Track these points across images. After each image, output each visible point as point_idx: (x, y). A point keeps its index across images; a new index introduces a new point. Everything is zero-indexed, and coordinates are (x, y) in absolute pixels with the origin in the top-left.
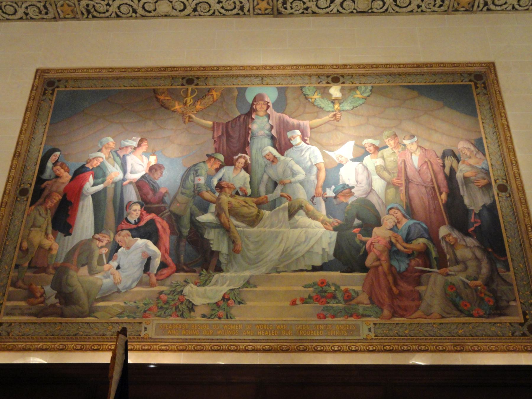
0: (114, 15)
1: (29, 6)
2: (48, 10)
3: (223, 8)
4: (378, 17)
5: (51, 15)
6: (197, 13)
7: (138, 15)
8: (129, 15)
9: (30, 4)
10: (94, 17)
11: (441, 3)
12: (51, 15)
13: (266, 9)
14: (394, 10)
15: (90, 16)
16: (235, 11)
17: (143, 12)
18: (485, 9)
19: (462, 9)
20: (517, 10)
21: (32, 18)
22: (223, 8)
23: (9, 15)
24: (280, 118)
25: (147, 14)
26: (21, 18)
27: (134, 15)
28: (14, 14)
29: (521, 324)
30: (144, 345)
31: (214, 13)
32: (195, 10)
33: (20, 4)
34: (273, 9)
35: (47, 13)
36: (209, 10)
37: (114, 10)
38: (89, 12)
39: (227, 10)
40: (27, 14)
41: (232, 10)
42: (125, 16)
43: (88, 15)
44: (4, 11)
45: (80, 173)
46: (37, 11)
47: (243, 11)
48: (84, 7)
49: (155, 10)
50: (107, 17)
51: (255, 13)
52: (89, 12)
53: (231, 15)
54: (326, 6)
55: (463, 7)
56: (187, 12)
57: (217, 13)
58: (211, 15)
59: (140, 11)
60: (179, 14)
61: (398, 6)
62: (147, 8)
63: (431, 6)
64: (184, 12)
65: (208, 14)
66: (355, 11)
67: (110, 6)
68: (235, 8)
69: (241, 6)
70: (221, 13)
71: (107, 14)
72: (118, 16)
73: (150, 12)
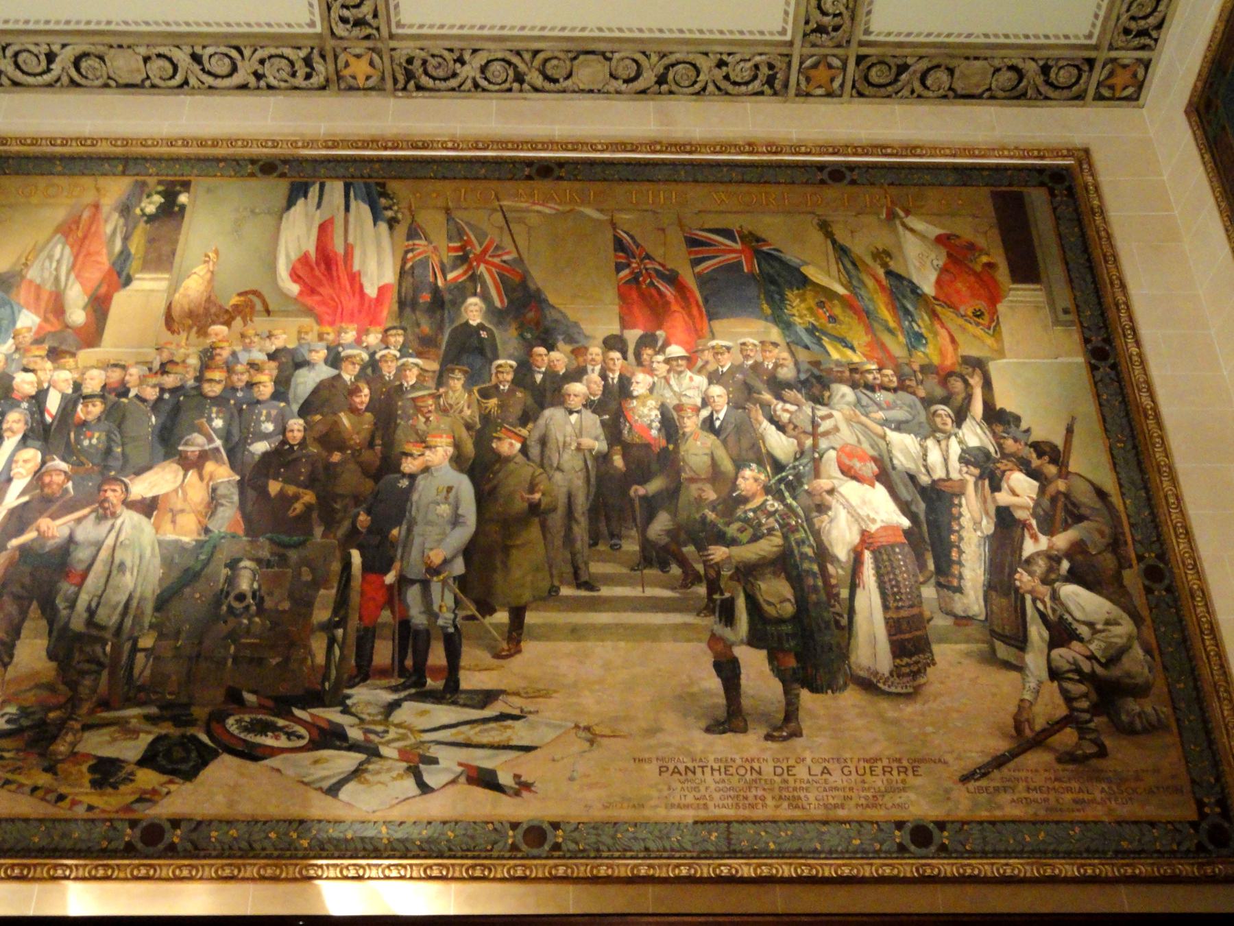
0: (469, 84)
1: (271, 57)
2: (313, 68)
3: (727, 77)
4: (352, 99)
5: (316, 80)
6: (664, 88)
7: (526, 86)
8: (507, 85)
9: (273, 51)
10: (419, 88)
11: (308, 70)
12: (316, 80)
13: (368, 78)
14: (203, 83)
15: (412, 84)
16: (756, 86)
17: (539, 81)
18: (412, 84)
19: (820, 91)
20: (484, 90)
21: (269, 87)
22: (727, 77)
23: (216, 76)
24: (594, 338)
25: (548, 85)
26: (244, 87)
27: (516, 86)
28: (230, 75)
29: (1194, 825)
30: (556, 866)
31: (704, 89)
32: (661, 80)
33: (247, 53)
34: (383, 79)
35: (308, 77)
36: (695, 82)
37: (472, 74)
38: (409, 75)
39: (735, 83)
40: (258, 76)
41: (747, 83)
42: (497, 87)
43: (407, 82)
44: (207, 66)
45: (499, 439)
46: (288, 69)
47: (772, 86)
48: (400, 65)
49: (569, 76)
50: (453, 90)
51: (839, 92)
52: (409, 75)
53: (229, 88)
54: (888, 80)
55: (820, 86)
56: (640, 84)
57: (711, 88)
58: (698, 93)
59: (536, 78)
60: (624, 87)
61: (1052, 85)
62: (168, 65)
63: (284, 75)
64: (635, 83)
65: (691, 90)
66: (112, 83)
67: (463, 63)
68: (755, 77)
69: (769, 76)
70: (719, 89)
71: (453, 83)
72: (74, 84)
73: (556, 81)
